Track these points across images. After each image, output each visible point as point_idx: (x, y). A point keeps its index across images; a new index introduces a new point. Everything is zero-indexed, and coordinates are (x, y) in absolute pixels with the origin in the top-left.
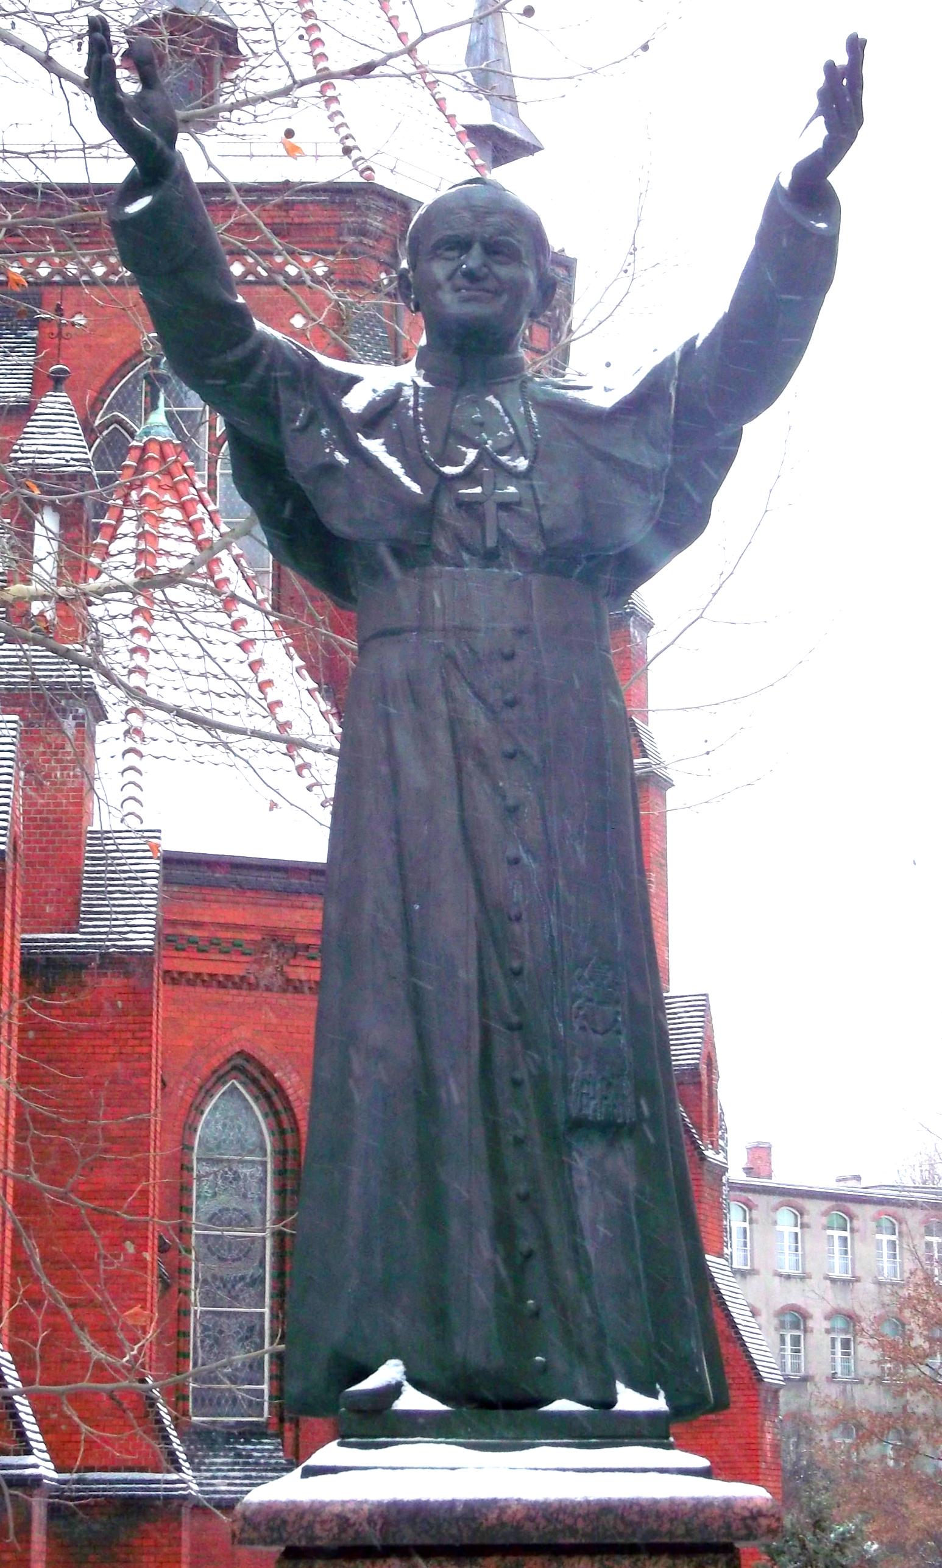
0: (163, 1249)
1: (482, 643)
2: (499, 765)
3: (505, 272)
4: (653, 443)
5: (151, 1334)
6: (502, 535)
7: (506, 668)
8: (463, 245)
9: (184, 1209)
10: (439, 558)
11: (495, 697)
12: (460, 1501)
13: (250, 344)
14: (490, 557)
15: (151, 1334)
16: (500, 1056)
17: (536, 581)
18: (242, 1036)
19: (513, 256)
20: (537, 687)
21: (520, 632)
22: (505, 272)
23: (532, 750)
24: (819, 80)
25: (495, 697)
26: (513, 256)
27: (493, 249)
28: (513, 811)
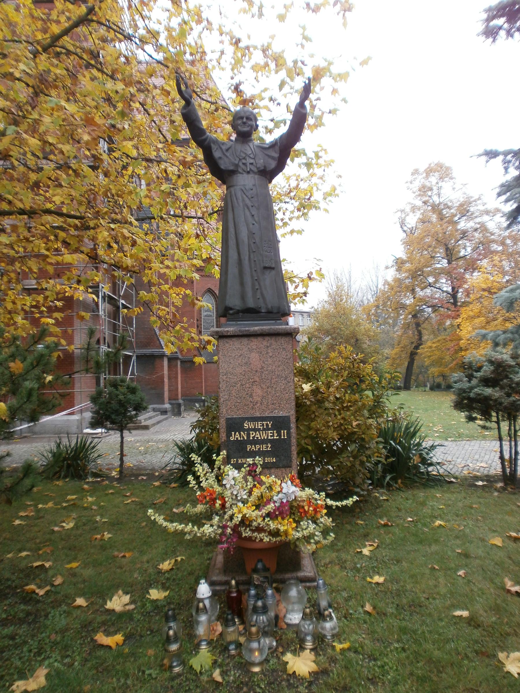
0: (197, 320)
1: (247, 187)
2: (250, 207)
3: (250, 123)
4: (276, 152)
5: (436, 653)
6: (250, 169)
7: (251, 192)
8: (242, 118)
9: (201, 314)
10: (240, 173)
11: (250, 196)
12: (211, 589)
13: (204, 137)
14: (248, 173)
15: (436, 653)
16: (252, 257)
17: (256, 176)
18: (209, 286)
19: (251, 120)
20: (257, 195)
21: (254, 185)
22: (250, 123)
23: (256, 205)
24: (318, 13)
25: (250, 196)
26: (251, 120)
27: (248, 118)
28: (253, 216)
